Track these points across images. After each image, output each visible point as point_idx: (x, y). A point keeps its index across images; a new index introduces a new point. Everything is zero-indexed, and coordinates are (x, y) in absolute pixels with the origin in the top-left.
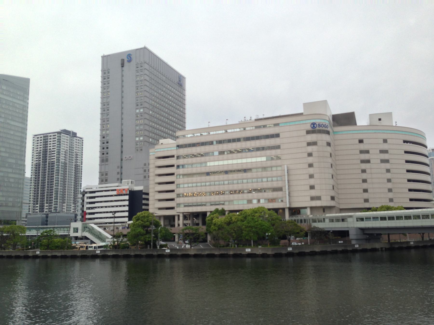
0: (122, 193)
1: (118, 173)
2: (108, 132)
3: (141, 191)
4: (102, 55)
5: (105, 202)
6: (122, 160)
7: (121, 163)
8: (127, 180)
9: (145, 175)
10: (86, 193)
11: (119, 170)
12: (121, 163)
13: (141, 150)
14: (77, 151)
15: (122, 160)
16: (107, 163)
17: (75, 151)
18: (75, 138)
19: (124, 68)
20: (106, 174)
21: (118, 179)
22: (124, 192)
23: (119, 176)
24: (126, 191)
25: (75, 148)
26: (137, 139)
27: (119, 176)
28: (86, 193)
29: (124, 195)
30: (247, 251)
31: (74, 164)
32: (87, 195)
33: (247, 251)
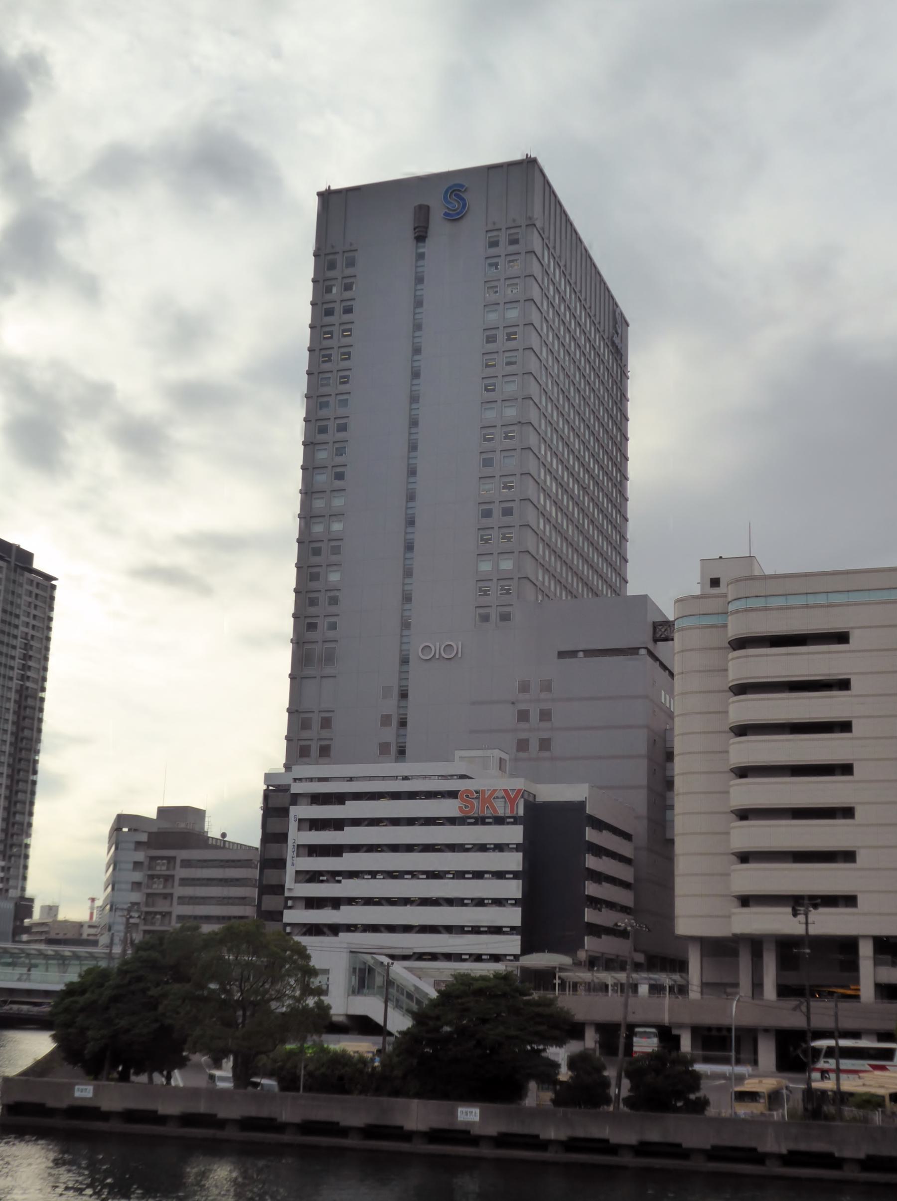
0: (488, 813)
1: (386, 720)
2: (337, 527)
3: (580, 806)
4: (323, 188)
5: (394, 848)
6: (405, 661)
7: (403, 675)
8: (479, 753)
9: (523, 736)
10: (295, 799)
11: (391, 706)
12: (403, 675)
13: (505, 617)
14: (31, 632)
15: (405, 661)
16: (328, 671)
17: (22, 629)
18: (27, 574)
19: (428, 248)
20: (326, 723)
21: (384, 749)
22: (501, 809)
23: (389, 735)
24: (513, 801)
25: (23, 618)
26: (486, 567)
27: (389, 735)
28: (295, 799)
29: (500, 821)
30: (77, 1094)
31: (15, 684)
32: (299, 812)
33: (77, 1094)
